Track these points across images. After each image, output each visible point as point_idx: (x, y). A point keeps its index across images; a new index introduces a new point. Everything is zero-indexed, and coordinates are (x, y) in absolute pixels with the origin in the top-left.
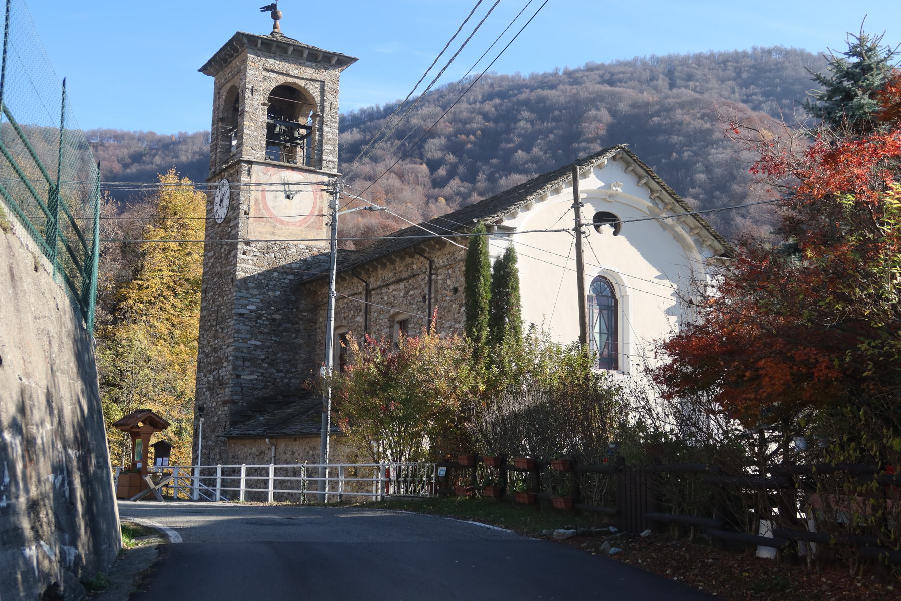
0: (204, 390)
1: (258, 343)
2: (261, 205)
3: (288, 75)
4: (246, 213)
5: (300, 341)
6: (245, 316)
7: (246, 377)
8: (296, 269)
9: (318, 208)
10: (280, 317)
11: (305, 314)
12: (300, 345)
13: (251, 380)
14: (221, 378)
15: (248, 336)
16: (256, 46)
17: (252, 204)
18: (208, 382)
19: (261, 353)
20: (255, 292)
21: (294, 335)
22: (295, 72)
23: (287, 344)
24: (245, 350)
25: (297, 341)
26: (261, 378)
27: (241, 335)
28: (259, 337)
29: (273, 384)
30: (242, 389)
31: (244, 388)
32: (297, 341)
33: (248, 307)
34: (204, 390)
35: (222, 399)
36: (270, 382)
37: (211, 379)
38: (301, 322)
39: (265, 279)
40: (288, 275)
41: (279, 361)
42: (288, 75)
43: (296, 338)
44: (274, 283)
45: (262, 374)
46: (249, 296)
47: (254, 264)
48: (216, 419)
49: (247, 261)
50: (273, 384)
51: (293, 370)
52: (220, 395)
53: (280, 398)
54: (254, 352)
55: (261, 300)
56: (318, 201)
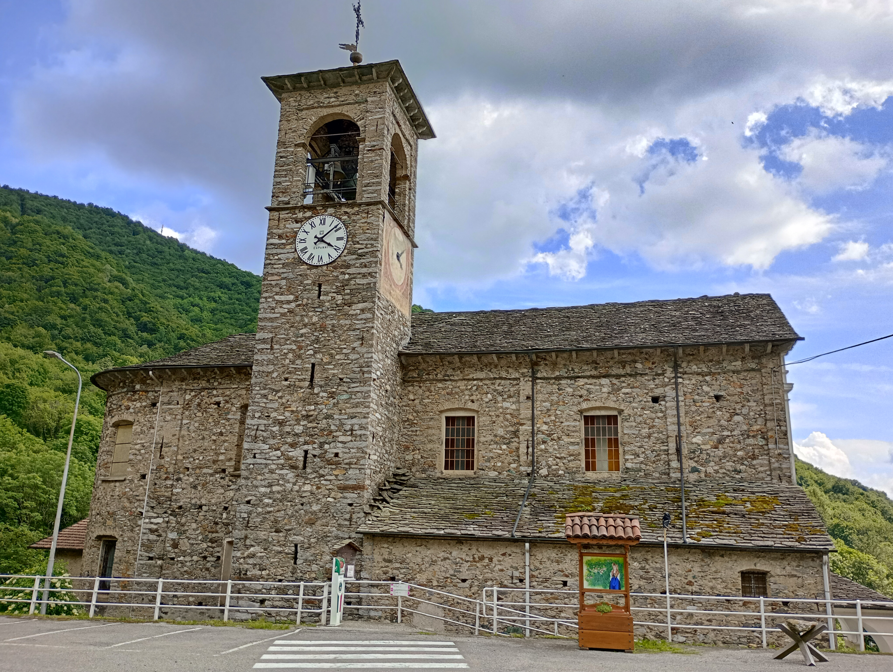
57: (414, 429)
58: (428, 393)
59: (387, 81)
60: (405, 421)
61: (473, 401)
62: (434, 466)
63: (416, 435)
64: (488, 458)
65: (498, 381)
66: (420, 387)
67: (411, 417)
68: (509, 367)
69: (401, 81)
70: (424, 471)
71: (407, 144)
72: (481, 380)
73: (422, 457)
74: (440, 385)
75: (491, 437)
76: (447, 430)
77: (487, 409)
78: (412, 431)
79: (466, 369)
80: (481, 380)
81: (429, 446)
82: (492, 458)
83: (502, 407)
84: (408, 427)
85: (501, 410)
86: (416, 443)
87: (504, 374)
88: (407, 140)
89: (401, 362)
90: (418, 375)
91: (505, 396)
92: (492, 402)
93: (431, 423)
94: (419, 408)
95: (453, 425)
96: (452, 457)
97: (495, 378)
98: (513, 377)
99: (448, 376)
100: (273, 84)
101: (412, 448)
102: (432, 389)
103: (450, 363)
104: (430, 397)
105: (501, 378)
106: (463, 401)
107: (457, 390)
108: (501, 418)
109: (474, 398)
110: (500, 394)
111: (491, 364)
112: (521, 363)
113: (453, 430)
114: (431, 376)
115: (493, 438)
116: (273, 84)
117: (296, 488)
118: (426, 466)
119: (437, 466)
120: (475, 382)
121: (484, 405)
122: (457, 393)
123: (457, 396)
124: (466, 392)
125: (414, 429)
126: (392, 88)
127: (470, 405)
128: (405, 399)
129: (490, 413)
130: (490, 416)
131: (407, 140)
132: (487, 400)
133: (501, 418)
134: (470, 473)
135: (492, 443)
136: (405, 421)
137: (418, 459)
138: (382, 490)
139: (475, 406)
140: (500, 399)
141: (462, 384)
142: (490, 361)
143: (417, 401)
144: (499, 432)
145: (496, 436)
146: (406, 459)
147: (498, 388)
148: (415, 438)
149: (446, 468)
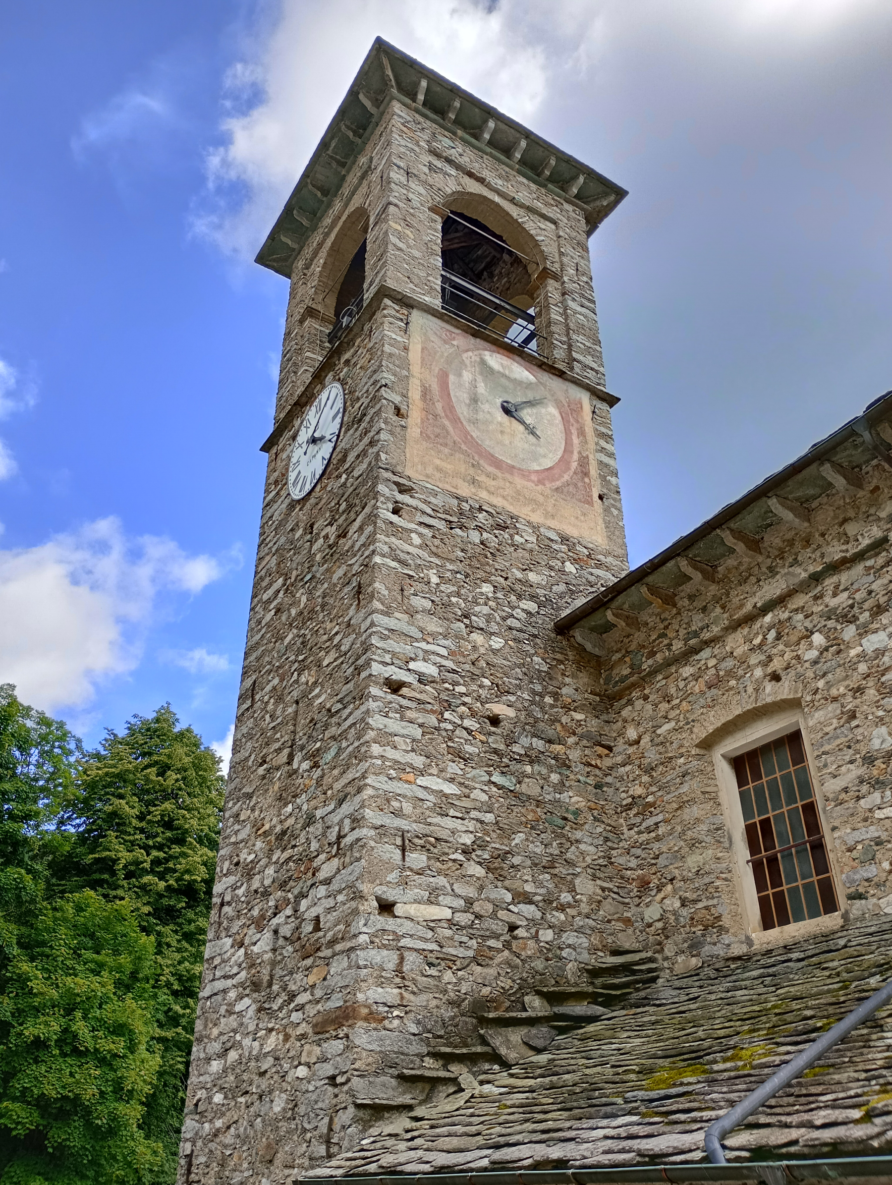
0: (232, 994)
1: (450, 789)
2: (439, 406)
3: (481, 180)
4: (398, 412)
5: (573, 799)
6: (404, 691)
7: (412, 910)
8: (539, 586)
9: (576, 456)
10: (511, 713)
11: (579, 716)
12: (577, 813)
13: (431, 925)
14: (308, 928)
15: (419, 761)
16: (414, 99)
17: (415, 394)
18: (252, 962)
19: (458, 824)
20: (433, 625)
21: (555, 778)
22: (499, 183)
23: (539, 803)
24: (407, 808)
25: (564, 797)
26: (464, 919)
27: (390, 753)
28: (454, 768)
29: (507, 945)
30: (402, 959)
31: (410, 957)
32: (564, 797)
33: (412, 665)
34: (232, 994)
35: (311, 1010)
36: (497, 937)
37: (263, 944)
38: (571, 740)
39: (458, 595)
40: (520, 597)
41: (516, 860)
42: (481, 180)
43: (561, 787)
44: (486, 610)
45: (469, 902)
46: (414, 632)
47: (424, 546)
48: (278, 1105)
49: (402, 533)
50: (507, 945)
51: (565, 897)
52: (302, 998)
53: (536, 1005)
54: (437, 820)
55: (452, 653)
56: (576, 441)
57: (650, 822)
58: (664, 706)
59: (393, 98)
60: (629, 807)
61: (776, 677)
62: (714, 925)
63: (658, 839)
64: (866, 850)
65: (829, 582)
66: (646, 698)
67: (639, 791)
68: (845, 520)
69: (553, 162)
70: (694, 947)
71: (536, 218)
72: (780, 601)
73: (684, 903)
74: (687, 671)
75: (856, 771)
76: (744, 797)
77: (821, 684)
78: (649, 830)
79: (733, 593)
80: (780, 601)
81: (693, 861)
82: (879, 842)
83: (862, 656)
84: (638, 820)
85: (863, 668)
86: (661, 861)
87: (835, 551)
88: (530, 209)
89: (581, 650)
90: (631, 667)
91: (865, 617)
92: (829, 655)
93: (685, 788)
94: (652, 756)
95: (757, 776)
96: (777, 883)
97: (816, 578)
98: (865, 542)
99: (696, 634)
100: (274, 260)
101: (654, 882)
102: (673, 691)
103: (691, 598)
104: (672, 714)
105: (834, 568)
106: (750, 690)
107: (729, 663)
108: (871, 693)
109: (777, 665)
110: (847, 618)
111: (791, 543)
112: (877, 488)
113: (759, 792)
114: (659, 657)
115: (862, 771)
116: (274, 260)
117: (157, 1051)
118: (698, 929)
119: (726, 921)
120: (768, 618)
121: (810, 674)
122: (730, 673)
123: (733, 683)
124: (754, 659)
125: (650, 822)
126: (417, 111)
127: (771, 693)
128: (620, 746)
129: (834, 692)
130: (835, 699)
131: (530, 209)
132: (813, 654)
133: (871, 693)
134: (829, 922)
135: (865, 788)
136: (629, 807)
137: (675, 913)
138: (483, 1021)
139: (784, 690)
140: (850, 632)
141: (737, 643)
142: (789, 536)
143: (646, 740)
144: (876, 744)
145: (869, 760)
146: (648, 920)
147: (833, 602)
148: (656, 846)
149: (767, 924)
